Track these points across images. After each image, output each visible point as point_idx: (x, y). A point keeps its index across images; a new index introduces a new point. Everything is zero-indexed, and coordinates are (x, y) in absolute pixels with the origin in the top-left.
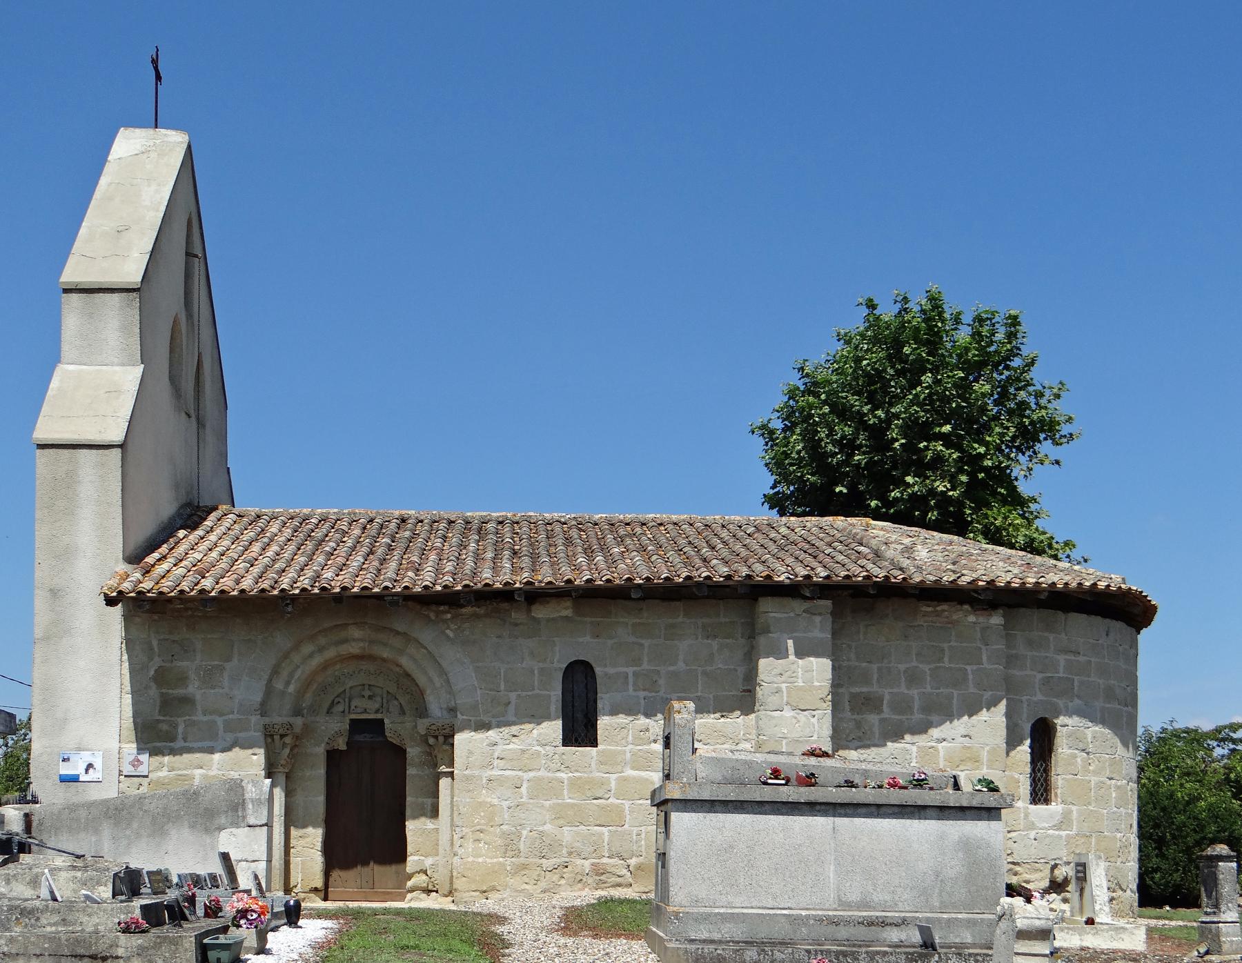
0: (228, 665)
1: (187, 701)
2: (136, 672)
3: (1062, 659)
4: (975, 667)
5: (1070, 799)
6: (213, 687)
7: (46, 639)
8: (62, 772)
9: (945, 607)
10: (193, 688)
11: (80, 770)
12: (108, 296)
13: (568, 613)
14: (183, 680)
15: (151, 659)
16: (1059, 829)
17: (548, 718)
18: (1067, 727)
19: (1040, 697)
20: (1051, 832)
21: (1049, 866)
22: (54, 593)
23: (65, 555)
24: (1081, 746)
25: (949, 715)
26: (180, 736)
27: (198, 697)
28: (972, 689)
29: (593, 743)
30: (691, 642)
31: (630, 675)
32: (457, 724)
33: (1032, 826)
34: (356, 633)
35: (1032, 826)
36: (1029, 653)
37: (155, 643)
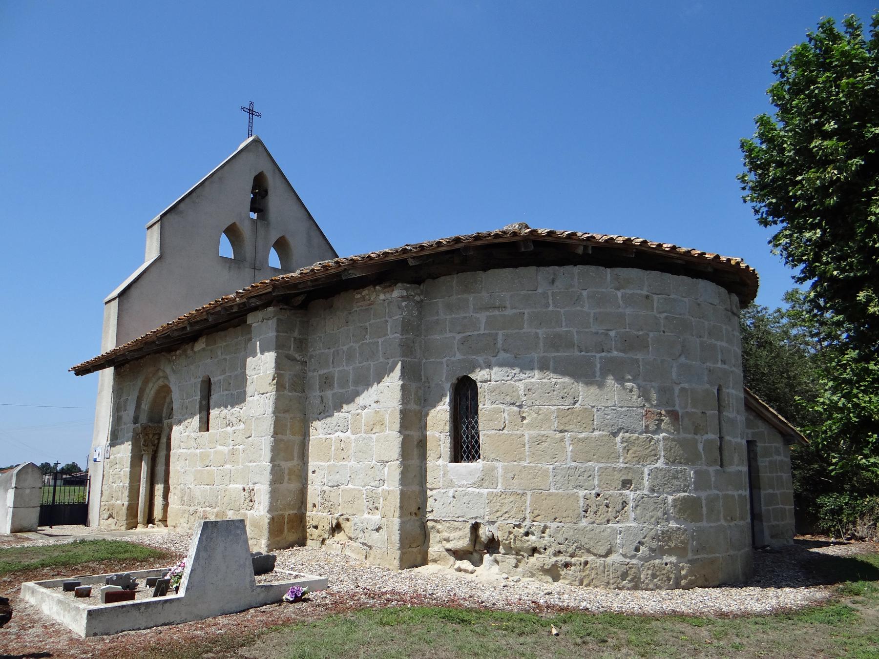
3: (483, 317)
4: (383, 339)
5: (493, 456)
9: (365, 292)
16: (480, 486)
18: (489, 379)
19: (458, 356)
20: (471, 490)
21: (469, 525)
24: (509, 399)
25: (368, 385)
28: (382, 360)
33: (451, 484)
35: (451, 484)
36: (448, 317)
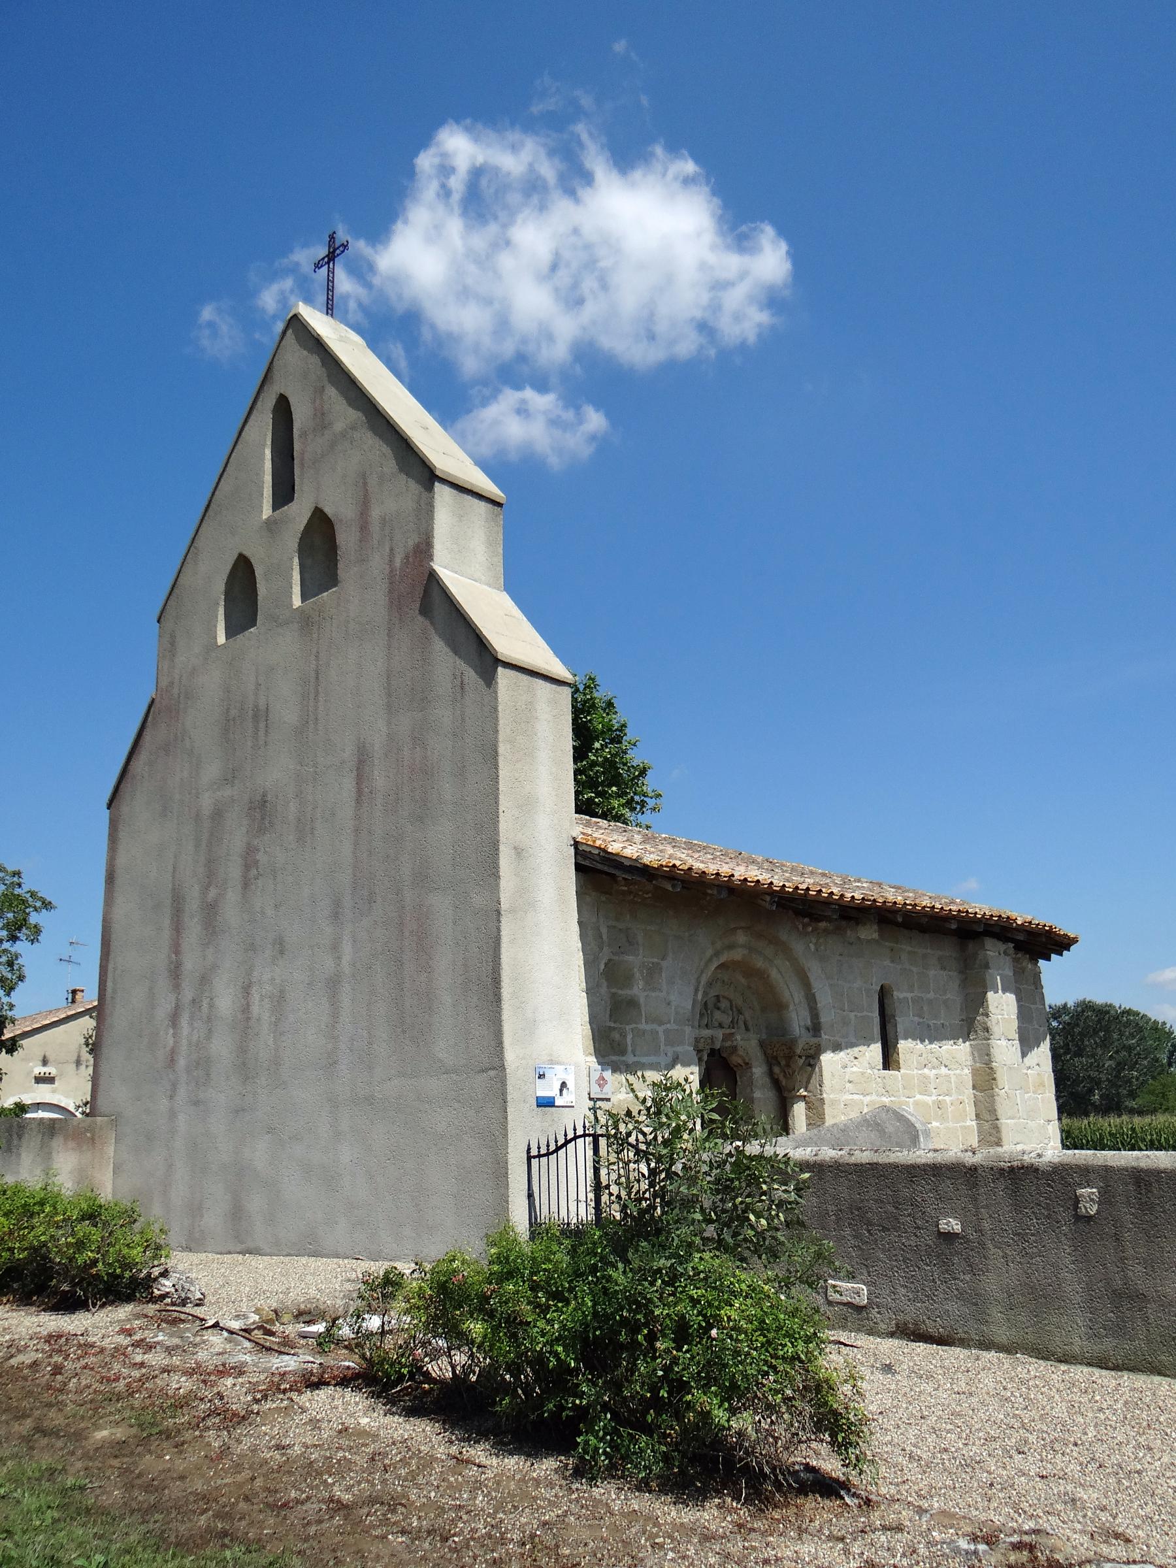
0: (664, 964)
1: (632, 1003)
2: (589, 964)
6: (654, 989)
7: (513, 911)
8: (540, 1094)
10: (638, 990)
11: (553, 1092)
12: (476, 501)
13: (876, 936)
14: (628, 980)
15: (601, 949)
17: (873, 1041)
22: (519, 852)
23: (528, 804)
26: (630, 1049)
27: (642, 1000)
29: (898, 1069)
30: (925, 976)
31: (661, 1034)
32: (823, 1044)
34: (741, 938)
37: (604, 930)
